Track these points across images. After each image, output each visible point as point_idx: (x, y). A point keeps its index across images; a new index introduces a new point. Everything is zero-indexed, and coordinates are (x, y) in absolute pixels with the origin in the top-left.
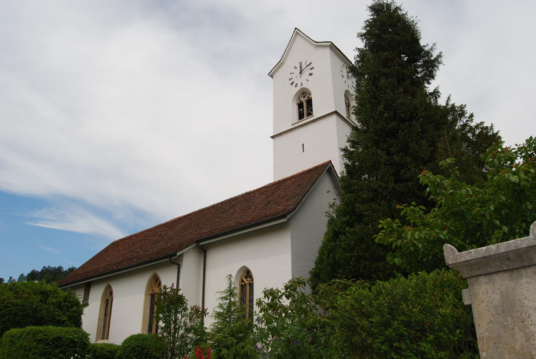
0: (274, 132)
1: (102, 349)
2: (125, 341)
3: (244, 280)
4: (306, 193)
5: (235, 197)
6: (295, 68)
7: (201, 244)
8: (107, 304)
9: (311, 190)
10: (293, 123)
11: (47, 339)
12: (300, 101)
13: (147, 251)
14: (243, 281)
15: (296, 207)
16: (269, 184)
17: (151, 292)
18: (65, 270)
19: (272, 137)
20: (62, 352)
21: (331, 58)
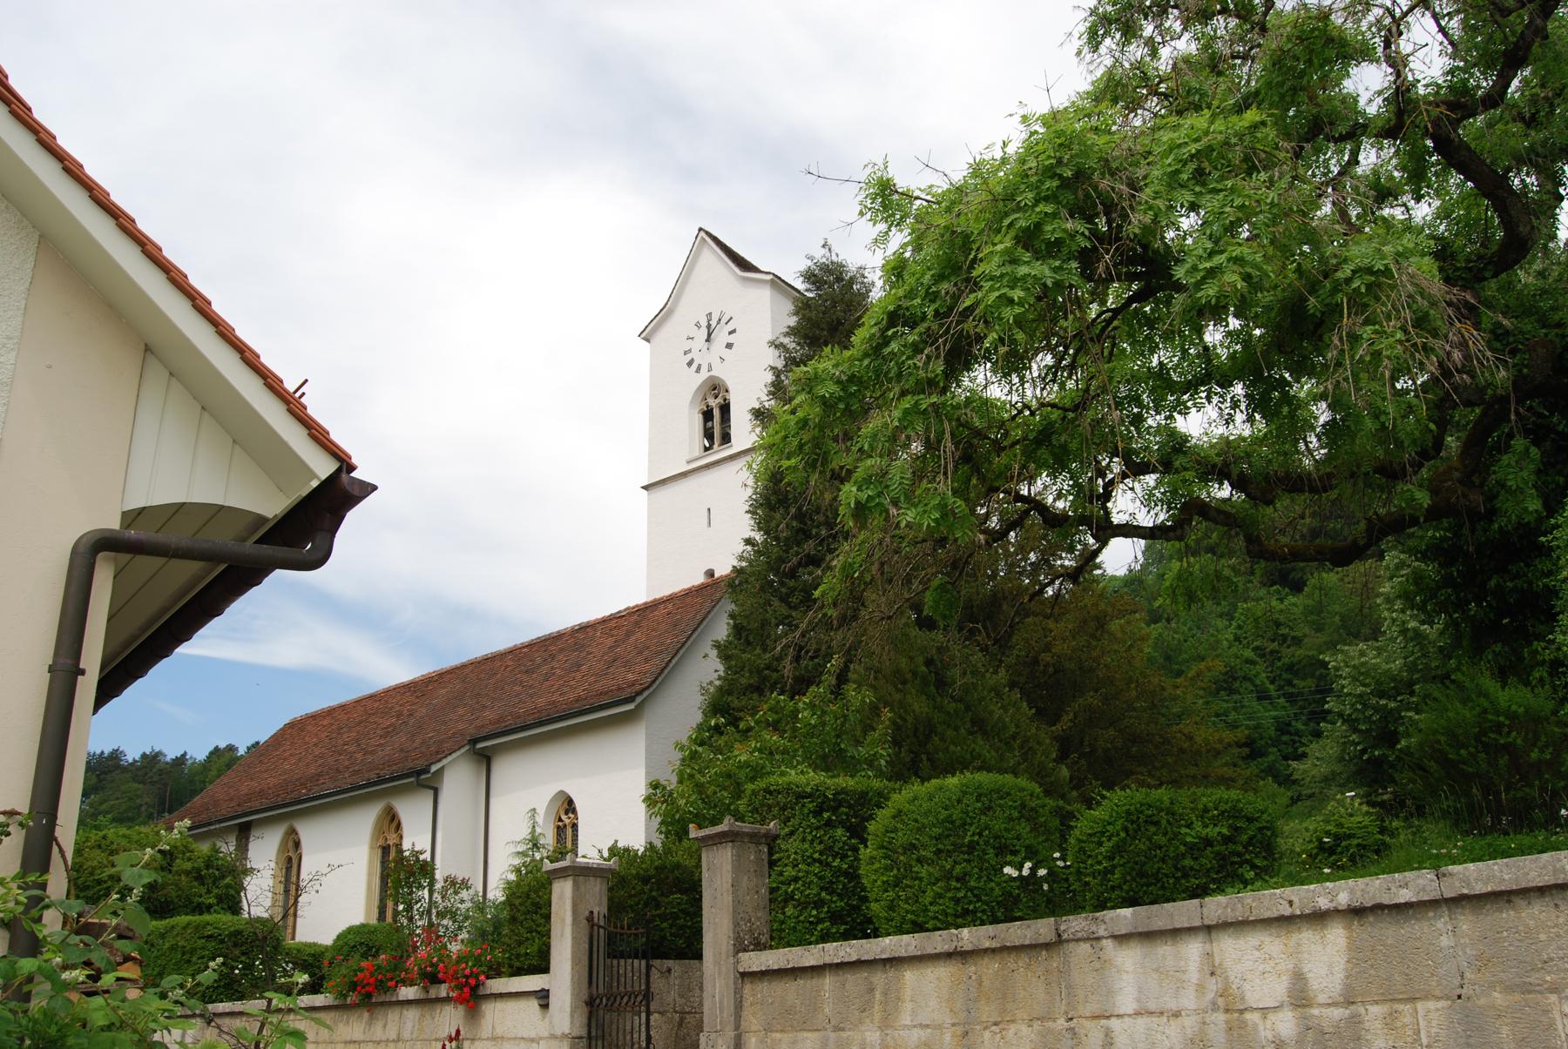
0: (650, 474)
1: (299, 951)
2: (338, 936)
3: (563, 817)
4: (681, 648)
5: (558, 632)
6: (698, 325)
7: (480, 745)
8: (288, 869)
9: (692, 639)
10: (688, 457)
11: (220, 935)
12: (708, 406)
13: (372, 753)
14: (560, 820)
15: (656, 678)
16: (625, 610)
17: (381, 842)
18: (131, 760)
19: (645, 488)
20: (243, 954)
21: (772, 311)
